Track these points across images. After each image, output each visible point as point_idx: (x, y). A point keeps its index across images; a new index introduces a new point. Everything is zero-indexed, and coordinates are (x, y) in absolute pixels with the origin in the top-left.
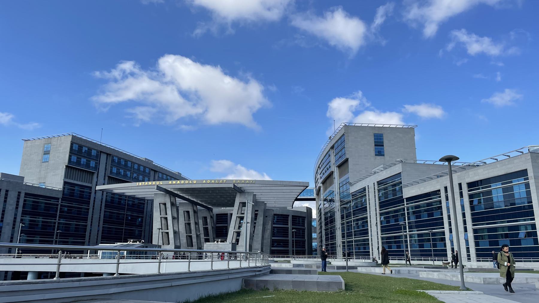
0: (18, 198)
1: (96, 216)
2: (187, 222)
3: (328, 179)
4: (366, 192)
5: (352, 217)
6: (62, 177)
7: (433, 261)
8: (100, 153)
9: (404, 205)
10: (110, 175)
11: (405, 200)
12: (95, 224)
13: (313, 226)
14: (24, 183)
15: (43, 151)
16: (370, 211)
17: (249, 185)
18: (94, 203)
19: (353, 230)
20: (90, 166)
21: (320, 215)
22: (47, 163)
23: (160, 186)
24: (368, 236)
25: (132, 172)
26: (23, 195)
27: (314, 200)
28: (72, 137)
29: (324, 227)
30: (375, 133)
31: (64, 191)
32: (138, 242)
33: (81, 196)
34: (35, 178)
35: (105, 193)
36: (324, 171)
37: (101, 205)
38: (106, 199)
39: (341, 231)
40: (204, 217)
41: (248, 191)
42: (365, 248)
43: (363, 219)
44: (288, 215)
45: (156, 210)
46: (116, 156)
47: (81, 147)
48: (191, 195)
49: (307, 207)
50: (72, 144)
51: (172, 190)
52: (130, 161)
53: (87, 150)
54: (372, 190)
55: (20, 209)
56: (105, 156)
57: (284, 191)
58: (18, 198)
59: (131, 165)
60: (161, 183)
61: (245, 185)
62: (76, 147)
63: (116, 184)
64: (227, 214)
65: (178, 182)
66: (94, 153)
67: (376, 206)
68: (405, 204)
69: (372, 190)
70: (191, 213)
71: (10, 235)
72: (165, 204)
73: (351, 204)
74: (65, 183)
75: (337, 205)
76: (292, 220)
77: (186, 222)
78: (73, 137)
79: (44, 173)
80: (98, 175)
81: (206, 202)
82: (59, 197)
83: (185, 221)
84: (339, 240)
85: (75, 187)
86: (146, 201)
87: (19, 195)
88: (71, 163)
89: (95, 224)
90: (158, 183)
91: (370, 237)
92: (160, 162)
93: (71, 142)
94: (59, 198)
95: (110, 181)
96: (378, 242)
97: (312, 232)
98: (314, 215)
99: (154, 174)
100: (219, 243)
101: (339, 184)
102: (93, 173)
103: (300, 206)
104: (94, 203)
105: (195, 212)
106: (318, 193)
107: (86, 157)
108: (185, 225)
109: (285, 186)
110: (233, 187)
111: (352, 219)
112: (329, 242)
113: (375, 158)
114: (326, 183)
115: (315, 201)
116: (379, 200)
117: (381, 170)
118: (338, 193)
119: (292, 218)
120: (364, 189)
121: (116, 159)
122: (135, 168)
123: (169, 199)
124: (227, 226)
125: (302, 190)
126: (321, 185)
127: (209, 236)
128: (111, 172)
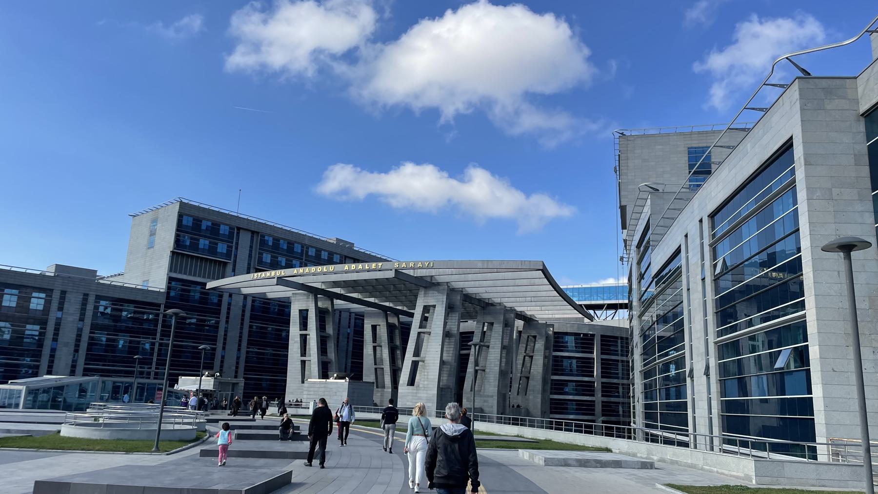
1: (233, 334)
8: (238, 233)
10: (258, 266)
12: (232, 346)
18: (228, 313)
20: (217, 252)
22: (152, 249)
25: (304, 261)
26: (91, 299)
28: (180, 205)
30: (690, 146)
31: (168, 293)
37: (243, 315)
38: (253, 306)
46: (270, 235)
47: (197, 222)
50: (180, 217)
51: (323, 287)
52: (298, 243)
53: (210, 225)
55: (221, 333)
56: (249, 235)
57: (518, 282)
59: (302, 251)
62: (188, 221)
66: (224, 230)
71: (70, 362)
74: (170, 280)
76: (602, 345)
78: (182, 204)
80: (234, 266)
82: (161, 303)
85: (190, 286)
88: (198, 251)
89: (232, 346)
92: (360, 246)
93: (179, 212)
94: (161, 304)
102: (225, 264)
104: (228, 313)
109: (498, 270)
116: (717, 291)
119: (602, 341)
122: (310, 253)
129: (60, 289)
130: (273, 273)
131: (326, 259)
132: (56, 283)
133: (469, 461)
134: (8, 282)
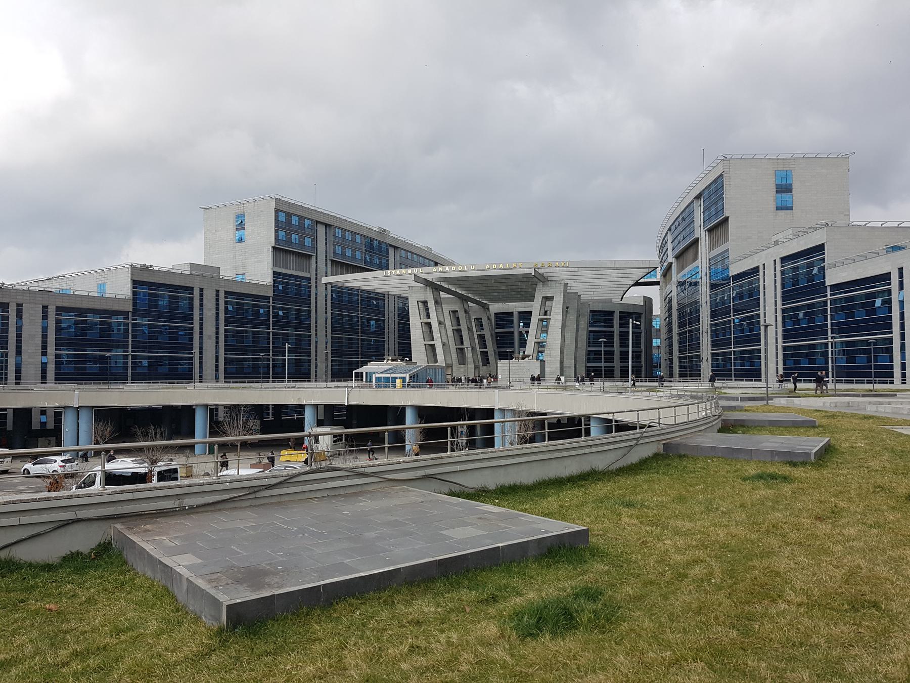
0: (217, 300)
1: (322, 321)
2: (456, 328)
3: (688, 251)
4: (759, 275)
5: (732, 314)
6: (269, 265)
7: (872, 384)
8: (317, 224)
9: (826, 296)
11: (828, 289)
12: (321, 333)
13: (653, 327)
14: (221, 277)
15: (234, 225)
16: (765, 305)
17: (557, 270)
19: (732, 336)
21: (670, 309)
23: (418, 275)
24: (760, 345)
26: (222, 295)
27: (657, 283)
29: (675, 330)
32: (399, 360)
33: (298, 294)
34: (229, 267)
35: (329, 287)
36: (680, 237)
39: (709, 336)
40: (452, 311)
41: (553, 278)
42: (752, 364)
43: (751, 317)
44: (613, 312)
45: (413, 311)
47: (289, 215)
48: (460, 287)
49: (644, 296)
50: (277, 211)
51: (434, 280)
54: (769, 272)
57: (615, 276)
58: (217, 300)
60: (421, 270)
61: (548, 270)
62: (282, 217)
63: (353, 273)
64: (512, 313)
65: (447, 269)
67: (776, 298)
68: (829, 295)
69: (769, 272)
70: (431, 304)
72: (425, 303)
73: (730, 294)
74: (275, 274)
75: (704, 294)
77: (454, 328)
79: (241, 259)
81: (475, 293)
83: (421, 319)
84: (706, 349)
86: (386, 296)
87: (217, 295)
89: (321, 333)
90: (416, 270)
91: (762, 347)
95: (333, 267)
96: (777, 354)
97: (653, 337)
98: (657, 309)
99: (394, 253)
100: (521, 361)
101: (710, 261)
103: (636, 295)
105: (437, 303)
106: (667, 272)
107: (298, 232)
108: (452, 333)
110: (533, 274)
111: (732, 317)
112: (687, 353)
113: (775, 214)
114: (682, 257)
115: (659, 285)
117: (789, 238)
118: (706, 275)
120: (756, 270)
121: (339, 233)
123: (432, 295)
124: (513, 330)
125: (645, 274)
126: (674, 260)
127: (487, 348)
128: (335, 253)
129: (199, 286)
130: (410, 271)
131: (284, 221)
132: (195, 281)
133: (201, 562)
134: (161, 282)
